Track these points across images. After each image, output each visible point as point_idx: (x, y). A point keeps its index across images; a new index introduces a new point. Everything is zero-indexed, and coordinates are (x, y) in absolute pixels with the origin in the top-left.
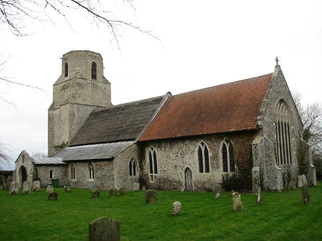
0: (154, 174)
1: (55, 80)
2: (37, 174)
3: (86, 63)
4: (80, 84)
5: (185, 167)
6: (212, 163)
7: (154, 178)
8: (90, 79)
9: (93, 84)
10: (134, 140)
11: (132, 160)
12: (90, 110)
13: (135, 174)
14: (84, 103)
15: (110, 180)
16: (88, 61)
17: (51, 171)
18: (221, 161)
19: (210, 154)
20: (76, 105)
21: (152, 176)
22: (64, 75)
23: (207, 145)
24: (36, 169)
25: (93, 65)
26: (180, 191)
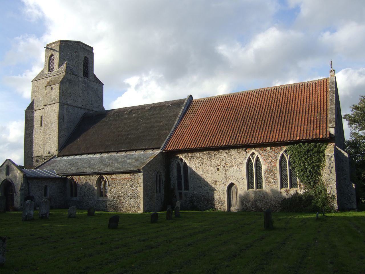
0: (184, 191)
1: (120, 97)
2: (29, 190)
3: (78, 56)
4: (70, 80)
5: (229, 182)
6: (268, 178)
7: (183, 196)
8: (82, 76)
9: (85, 83)
10: (159, 148)
11: (158, 173)
12: (82, 112)
13: (160, 192)
14: (75, 105)
15: (134, 198)
16: (80, 54)
17: (46, 187)
18: (278, 175)
19: (264, 167)
20: (66, 106)
21: (181, 194)
22: (47, 70)
23: (259, 156)
24: (28, 184)
25: (85, 59)
26: (175, 212)
